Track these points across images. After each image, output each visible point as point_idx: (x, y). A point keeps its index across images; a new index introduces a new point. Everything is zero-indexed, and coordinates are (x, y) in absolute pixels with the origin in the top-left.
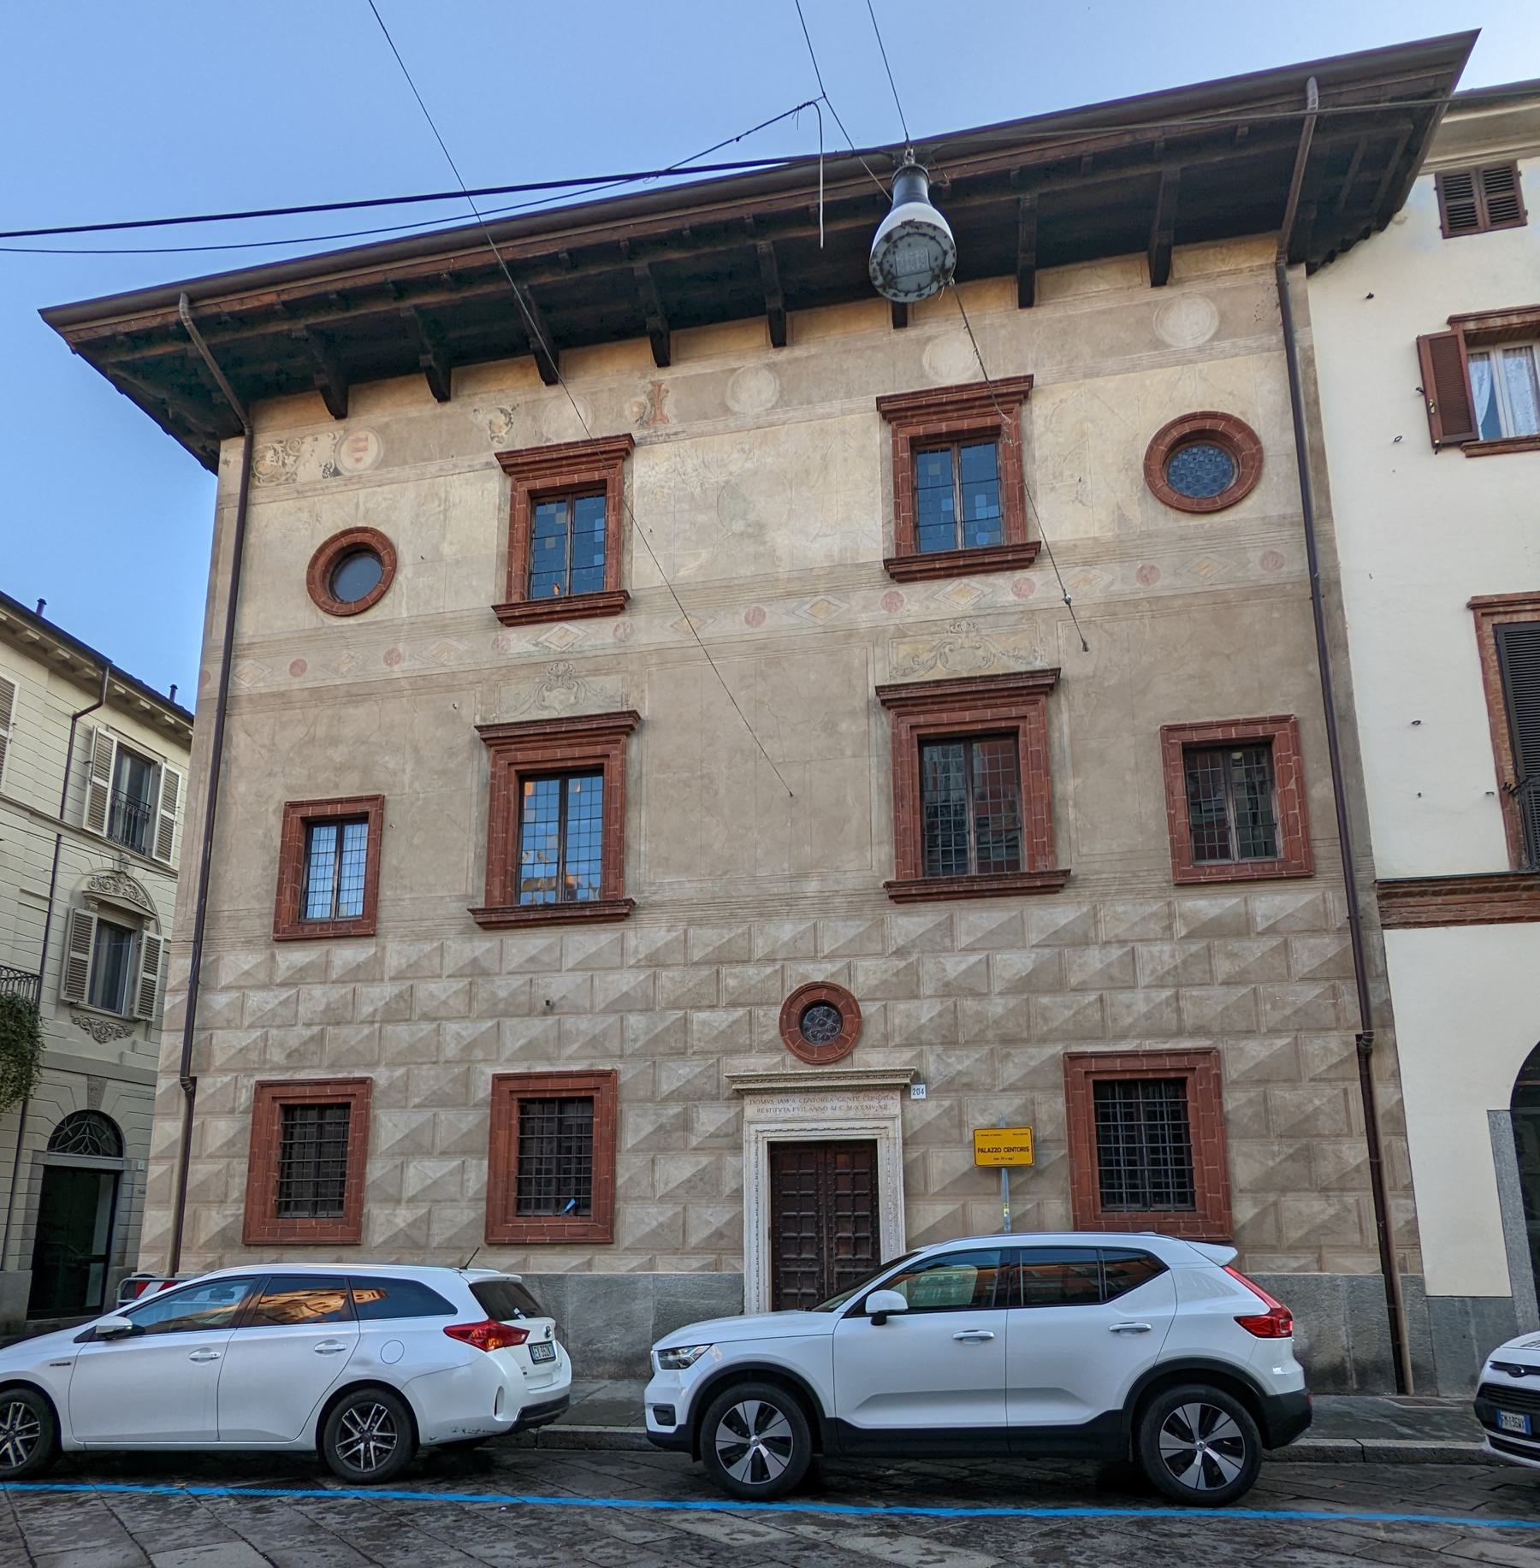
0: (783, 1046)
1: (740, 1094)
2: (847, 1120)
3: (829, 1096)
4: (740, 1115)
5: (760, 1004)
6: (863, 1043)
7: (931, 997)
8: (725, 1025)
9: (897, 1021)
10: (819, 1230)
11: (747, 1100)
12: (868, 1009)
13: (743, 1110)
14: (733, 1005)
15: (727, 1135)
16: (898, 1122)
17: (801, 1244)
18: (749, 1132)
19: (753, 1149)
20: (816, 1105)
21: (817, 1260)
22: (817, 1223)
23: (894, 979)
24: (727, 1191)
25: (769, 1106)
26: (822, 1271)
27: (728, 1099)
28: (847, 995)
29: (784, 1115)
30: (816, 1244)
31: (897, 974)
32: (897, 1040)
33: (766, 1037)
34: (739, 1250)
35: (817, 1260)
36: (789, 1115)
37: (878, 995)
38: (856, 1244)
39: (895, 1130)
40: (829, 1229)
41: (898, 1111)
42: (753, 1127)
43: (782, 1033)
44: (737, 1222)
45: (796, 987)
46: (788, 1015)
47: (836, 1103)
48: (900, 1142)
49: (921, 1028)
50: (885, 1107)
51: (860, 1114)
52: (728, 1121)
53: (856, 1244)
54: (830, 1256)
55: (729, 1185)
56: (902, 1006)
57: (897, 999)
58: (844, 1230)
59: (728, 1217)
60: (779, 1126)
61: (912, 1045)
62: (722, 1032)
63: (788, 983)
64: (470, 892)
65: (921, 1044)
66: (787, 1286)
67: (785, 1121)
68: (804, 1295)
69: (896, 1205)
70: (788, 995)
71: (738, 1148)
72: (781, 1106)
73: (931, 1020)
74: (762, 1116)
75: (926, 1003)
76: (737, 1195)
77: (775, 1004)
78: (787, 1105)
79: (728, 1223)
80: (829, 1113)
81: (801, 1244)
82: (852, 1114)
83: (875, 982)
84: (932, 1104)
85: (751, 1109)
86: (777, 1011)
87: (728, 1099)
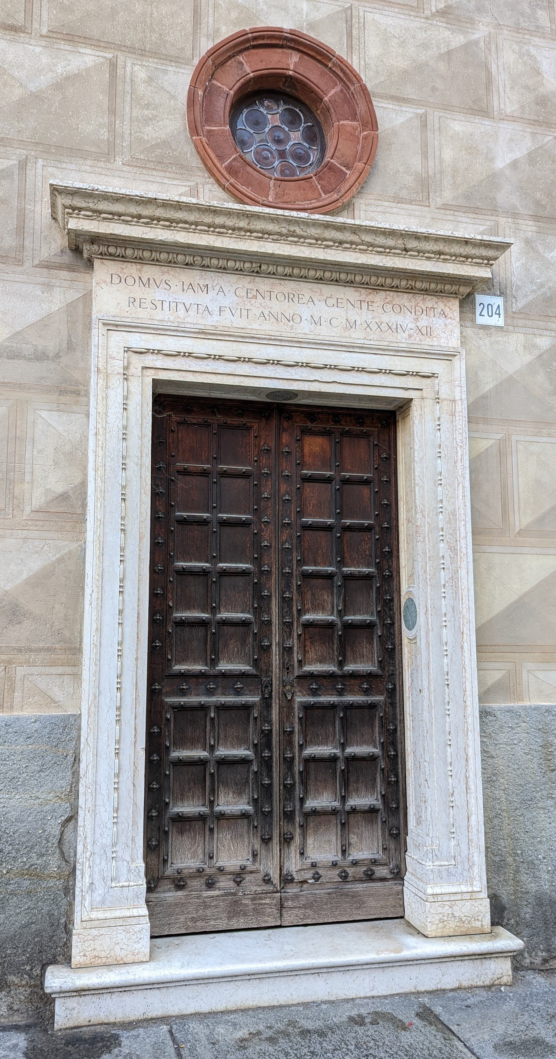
0: (196, 162)
1: (84, 251)
2: (350, 348)
3: (306, 289)
4: (79, 315)
5: (141, 52)
6: (377, 184)
7: (513, 119)
8: (44, 81)
9: (448, 154)
10: (260, 604)
11: (103, 270)
12: (391, 117)
13: (87, 298)
14: (70, 36)
15: (40, 356)
16: (460, 365)
17: (213, 637)
18: (108, 349)
19: (116, 395)
20: (277, 306)
21: (256, 679)
22: (257, 588)
23: (442, 67)
24: (37, 498)
25: (159, 294)
26: (267, 702)
27: (48, 266)
28: (344, 74)
29: (194, 320)
30: (252, 635)
31: (448, 55)
32: (448, 195)
33: (151, 133)
34: (67, 652)
35: (256, 679)
36: (209, 322)
37: (410, 91)
38: (346, 637)
39: (452, 382)
40: (286, 602)
41: (272, 444)
42: (119, 340)
43: (194, 129)
44: (67, 580)
45: (227, 32)
46: (210, 92)
47: (322, 309)
48: (462, 409)
49: (493, 180)
50: (429, 332)
51: (373, 338)
52: (44, 324)
53: (346, 637)
54: (286, 667)
55: (44, 482)
56: (459, 125)
57: (447, 107)
58: (316, 607)
59: (35, 565)
60: (186, 345)
61: (476, 210)
62: (37, 98)
63: (208, 21)
64: (180, 964)
65: (494, 210)
66: (180, 743)
67: (203, 334)
68: (223, 762)
69: (453, 550)
70: (206, 45)
71: (71, 391)
72: (189, 298)
73: (514, 165)
74: (143, 315)
75: (506, 130)
76: (68, 510)
77: (176, 60)
78: (204, 299)
79: (40, 581)
80: (304, 329)
81: (213, 637)
82: (357, 336)
83: (402, 64)
84: (515, 340)
85: (111, 290)
86: (180, 80)
87: (48, 266)
